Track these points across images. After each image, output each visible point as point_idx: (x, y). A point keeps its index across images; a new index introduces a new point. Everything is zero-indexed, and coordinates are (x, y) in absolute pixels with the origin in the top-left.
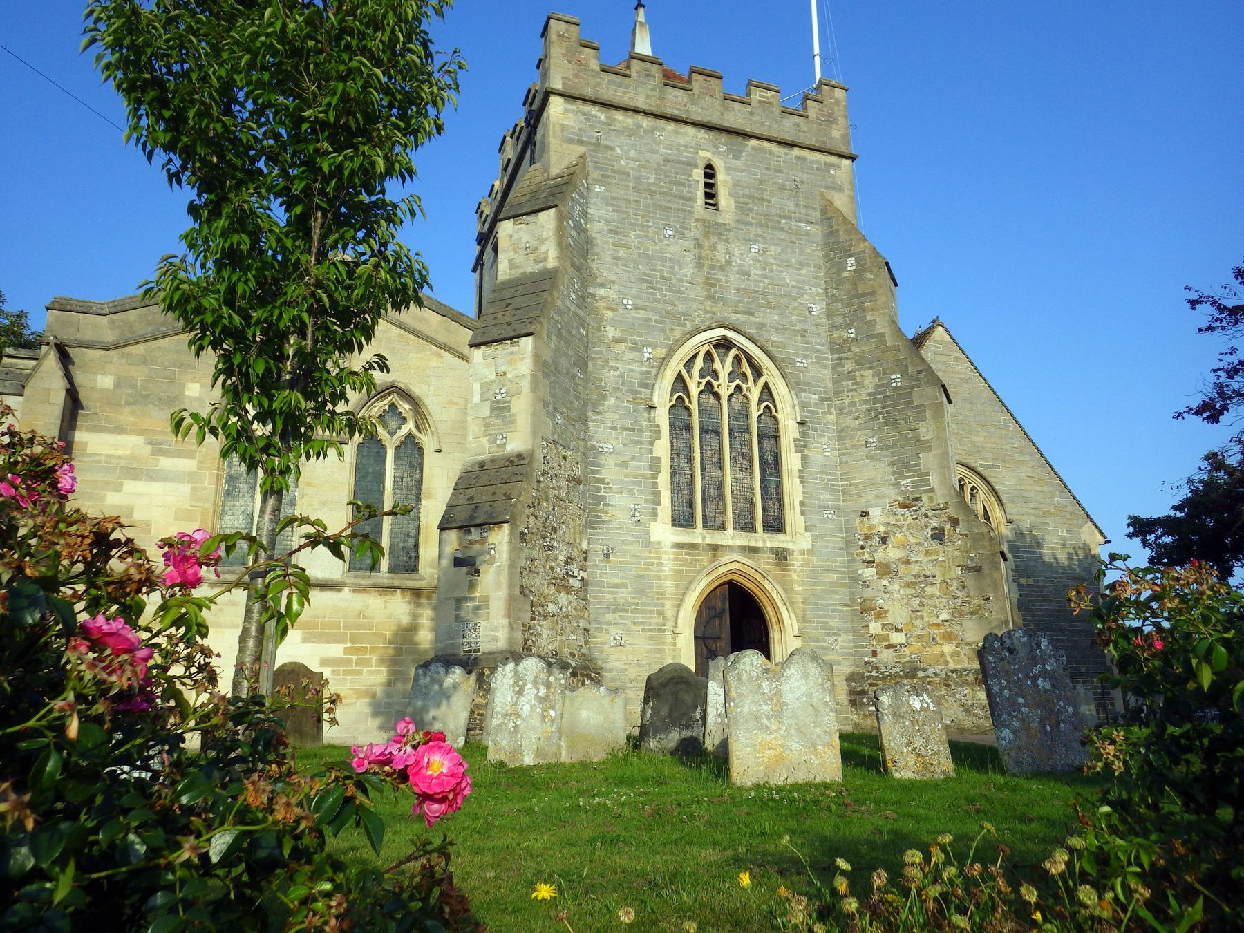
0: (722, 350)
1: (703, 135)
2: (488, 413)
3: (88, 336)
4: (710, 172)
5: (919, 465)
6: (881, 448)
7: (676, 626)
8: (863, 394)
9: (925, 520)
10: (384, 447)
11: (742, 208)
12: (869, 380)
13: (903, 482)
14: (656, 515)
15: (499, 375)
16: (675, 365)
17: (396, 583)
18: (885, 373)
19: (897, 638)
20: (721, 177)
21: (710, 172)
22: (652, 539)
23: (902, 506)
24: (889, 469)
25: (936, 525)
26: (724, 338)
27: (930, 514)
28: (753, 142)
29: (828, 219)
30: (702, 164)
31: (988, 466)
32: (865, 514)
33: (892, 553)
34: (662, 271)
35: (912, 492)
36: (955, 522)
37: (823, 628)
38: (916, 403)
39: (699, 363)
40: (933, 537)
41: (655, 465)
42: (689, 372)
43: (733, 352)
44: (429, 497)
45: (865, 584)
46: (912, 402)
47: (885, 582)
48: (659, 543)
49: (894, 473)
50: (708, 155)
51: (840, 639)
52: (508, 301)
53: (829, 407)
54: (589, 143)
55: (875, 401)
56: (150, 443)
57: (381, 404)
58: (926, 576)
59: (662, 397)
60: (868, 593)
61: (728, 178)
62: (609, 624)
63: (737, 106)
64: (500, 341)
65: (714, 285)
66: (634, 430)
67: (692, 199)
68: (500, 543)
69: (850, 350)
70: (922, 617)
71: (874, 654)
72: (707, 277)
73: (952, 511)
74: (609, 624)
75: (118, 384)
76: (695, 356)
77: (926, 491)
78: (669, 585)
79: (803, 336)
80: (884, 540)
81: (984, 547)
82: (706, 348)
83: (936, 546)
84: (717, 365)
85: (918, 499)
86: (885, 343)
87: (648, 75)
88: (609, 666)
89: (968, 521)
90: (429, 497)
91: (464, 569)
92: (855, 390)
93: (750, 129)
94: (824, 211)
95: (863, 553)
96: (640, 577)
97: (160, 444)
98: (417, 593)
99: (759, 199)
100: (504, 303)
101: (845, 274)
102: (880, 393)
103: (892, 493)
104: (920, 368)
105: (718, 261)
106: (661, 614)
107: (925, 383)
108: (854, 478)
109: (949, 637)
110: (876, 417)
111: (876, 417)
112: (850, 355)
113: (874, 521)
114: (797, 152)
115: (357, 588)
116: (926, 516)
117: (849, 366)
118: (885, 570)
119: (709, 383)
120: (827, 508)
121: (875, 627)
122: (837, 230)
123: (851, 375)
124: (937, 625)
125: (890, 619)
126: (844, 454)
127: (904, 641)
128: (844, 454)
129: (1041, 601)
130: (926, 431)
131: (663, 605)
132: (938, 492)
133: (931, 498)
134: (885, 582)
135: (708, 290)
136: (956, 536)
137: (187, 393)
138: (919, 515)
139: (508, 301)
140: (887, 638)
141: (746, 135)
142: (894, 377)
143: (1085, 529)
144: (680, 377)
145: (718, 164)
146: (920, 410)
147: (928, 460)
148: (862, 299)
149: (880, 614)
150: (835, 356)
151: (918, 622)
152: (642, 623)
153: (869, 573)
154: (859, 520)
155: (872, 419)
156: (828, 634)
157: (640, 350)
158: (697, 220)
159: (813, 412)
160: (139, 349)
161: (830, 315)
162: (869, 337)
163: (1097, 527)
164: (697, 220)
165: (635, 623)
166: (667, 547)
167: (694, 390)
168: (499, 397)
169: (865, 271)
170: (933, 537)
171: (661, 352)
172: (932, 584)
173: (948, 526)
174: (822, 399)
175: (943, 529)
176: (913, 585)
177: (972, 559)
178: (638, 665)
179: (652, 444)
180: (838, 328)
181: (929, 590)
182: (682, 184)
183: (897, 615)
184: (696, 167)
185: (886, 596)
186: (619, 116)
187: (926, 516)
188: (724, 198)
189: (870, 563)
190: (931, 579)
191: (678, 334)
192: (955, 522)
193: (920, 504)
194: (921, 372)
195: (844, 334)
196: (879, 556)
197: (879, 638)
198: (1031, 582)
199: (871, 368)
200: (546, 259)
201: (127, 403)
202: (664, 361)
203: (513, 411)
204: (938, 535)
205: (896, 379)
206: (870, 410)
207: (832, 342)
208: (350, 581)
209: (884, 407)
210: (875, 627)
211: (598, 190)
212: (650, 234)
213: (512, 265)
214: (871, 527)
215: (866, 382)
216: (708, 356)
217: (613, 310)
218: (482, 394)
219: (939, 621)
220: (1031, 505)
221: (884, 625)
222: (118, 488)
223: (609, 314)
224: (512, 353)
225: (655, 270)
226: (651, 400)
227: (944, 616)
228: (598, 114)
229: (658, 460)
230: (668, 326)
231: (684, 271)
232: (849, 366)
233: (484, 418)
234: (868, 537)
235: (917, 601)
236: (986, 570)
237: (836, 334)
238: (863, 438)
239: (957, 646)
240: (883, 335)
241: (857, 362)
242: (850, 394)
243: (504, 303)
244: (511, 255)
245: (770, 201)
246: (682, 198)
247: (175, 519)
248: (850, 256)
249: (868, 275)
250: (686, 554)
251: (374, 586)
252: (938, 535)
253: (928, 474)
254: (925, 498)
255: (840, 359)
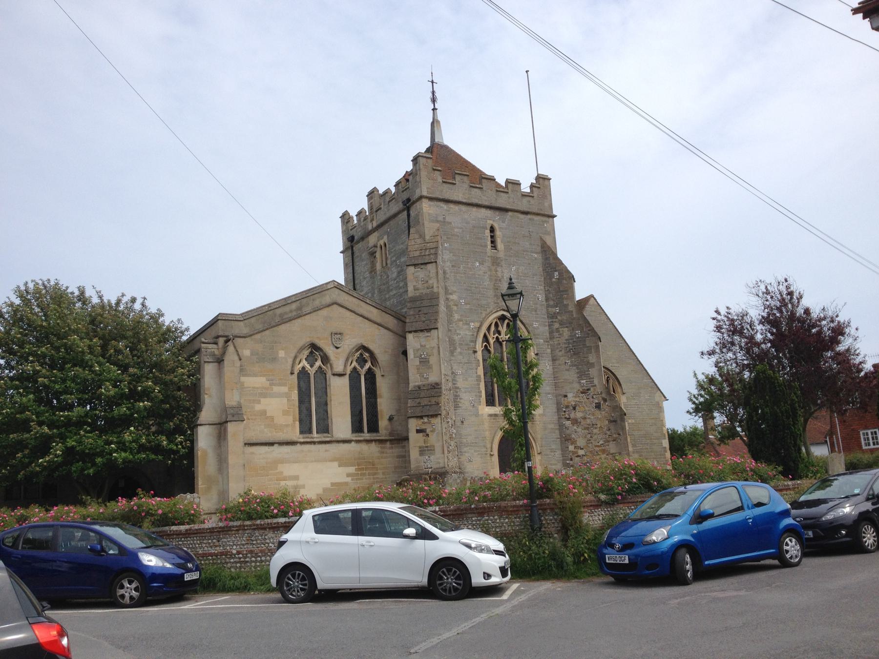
0: (501, 321)
1: (489, 213)
2: (418, 363)
3: (236, 332)
4: (492, 230)
5: (589, 374)
6: (572, 366)
7: (491, 451)
8: (563, 340)
9: (592, 400)
10: (360, 375)
11: (507, 248)
12: (566, 333)
13: (582, 381)
14: (480, 402)
15: (421, 346)
16: (484, 330)
17: (372, 438)
18: (573, 330)
19: (581, 452)
20: (498, 233)
21: (492, 230)
22: (480, 413)
23: (582, 393)
24: (576, 375)
25: (597, 401)
26: (503, 315)
27: (594, 397)
28: (510, 213)
29: (545, 251)
30: (489, 227)
31: (614, 366)
32: (566, 396)
33: (579, 415)
34: (475, 284)
35: (586, 387)
36: (605, 400)
37: (549, 449)
38: (588, 345)
39: (493, 328)
40: (596, 407)
41: (479, 380)
42: (489, 333)
43: (506, 321)
44: (381, 397)
45: (567, 428)
46: (586, 345)
47: (575, 428)
48: (482, 415)
49: (578, 377)
50: (491, 222)
51: (556, 454)
52: (420, 309)
53: (548, 345)
54: (440, 221)
55: (569, 343)
56: (268, 380)
57: (357, 354)
58: (593, 425)
59: (479, 347)
60: (568, 432)
61: (500, 233)
62: (465, 452)
63: (502, 194)
64: (422, 331)
65: (497, 289)
66: (469, 363)
67: (486, 246)
68: (438, 423)
69: (557, 318)
70: (592, 443)
71: (571, 459)
72: (494, 286)
73: (604, 395)
74: (465, 452)
75: (252, 354)
76: (490, 326)
77: (592, 386)
78: (487, 434)
79: (536, 311)
80: (574, 408)
81: (618, 412)
82: (496, 320)
83: (597, 412)
84: (500, 328)
85: (588, 390)
86: (573, 315)
87: (463, 182)
88: (466, 471)
89: (610, 400)
90: (381, 397)
91: (421, 434)
92: (560, 338)
93: (508, 207)
94: (542, 247)
95: (565, 415)
96: (476, 431)
97: (272, 380)
98: (381, 441)
99: (514, 243)
100: (417, 310)
101: (554, 280)
102: (571, 339)
103: (576, 386)
104: (589, 329)
105: (498, 277)
106: (485, 446)
107: (591, 336)
108: (560, 379)
109: (604, 451)
110: (569, 351)
111: (569, 351)
112: (557, 320)
113: (570, 400)
114: (529, 216)
115: (358, 441)
116: (593, 398)
117: (556, 325)
118: (575, 422)
119: (497, 337)
120: (549, 394)
121: (571, 448)
122: (549, 257)
123: (557, 330)
124: (598, 446)
125: (578, 444)
126: (556, 368)
127: (584, 454)
128: (556, 368)
129: (638, 430)
130: (592, 358)
131: (486, 442)
132: (598, 387)
133: (594, 389)
134: (575, 428)
135: (495, 292)
136: (604, 406)
137: (280, 356)
138: (590, 397)
139: (420, 309)
140: (576, 453)
141: (506, 210)
142: (577, 332)
143: (657, 394)
144: (485, 336)
145: (496, 226)
146: (589, 348)
147: (593, 372)
148: (562, 293)
149: (573, 442)
150: (550, 320)
151: (590, 445)
152: (479, 451)
153: (568, 423)
154: (563, 399)
155: (568, 352)
156: (552, 452)
157: (469, 324)
158: (488, 257)
159: (541, 348)
160: (258, 336)
161: (547, 300)
162: (566, 312)
163: (662, 393)
164: (488, 257)
165: (475, 451)
166: (486, 417)
167: (492, 341)
168: (423, 356)
169: (563, 279)
170: (596, 407)
171: (477, 325)
172: (596, 428)
173: (602, 402)
174: (544, 341)
175: (600, 403)
176: (587, 429)
177: (613, 417)
178: (477, 470)
179: (477, 369)
180: (552, 307)
181: (595, 431)
182: (481, 239)
183: (581, 442)
184: (487, 229)
185: (576, 434)
186: (452, 206)
187: (593, 398)
188: (500, 245)
189: (568, 419)
190: (595, 426)
191: (484, 315)
192: (605, 400)
193: (589, 392)
194: (589, 330)
195: (554, 310)
196: (572, 416)
197: (574, 453)
198: (633, 421)
199: (567, 327)
200: (432, 287)
201: (257, 362)
202: (479, 328)
203: (431, 362)
204: (598, 406)
205: (578, 333)
206: (566, 347)
207: (548, 313)
208: (354, 439)
209: (573, 346)
210: (571, 448)
211: (446, 245)
212: (469, 266)
213: (416, 289)
214: (569, 402)
215: (565, 334)
216: (496, 325)
217: (456, 305)
218: (414, 354)
219: (599, 444)
220: (633, 384)
221: (575, 447)
222: (259, 402)
223: (455, 308)
224: (428, 336)
225: (472, 284)
226: (475, 348)
227: (601, 442)
228: (443, 205)
229: (480, 376)
230: (480, 311)
231: (485, 283)
232: (556, 325)
233: (417, 366)
234: (567, 407)
235: (589, 435)
236: (619, 422)
237: (550, 309)
238: (564, 361)
239: (607, 455)
240: (572, 311)
241: (561, 324)
242: (557, 339)
243: (417, 310)
244: (415, 283)
245: (519, 244)
246: (482, 246)
247: (283, 415)
248: (556, 271)
249: (564, 282)
250: (494, 419)
251: (375, 441)
252: (598, 406)
253: (593, 378)
254: (592, 389)
255: (552, 322)
